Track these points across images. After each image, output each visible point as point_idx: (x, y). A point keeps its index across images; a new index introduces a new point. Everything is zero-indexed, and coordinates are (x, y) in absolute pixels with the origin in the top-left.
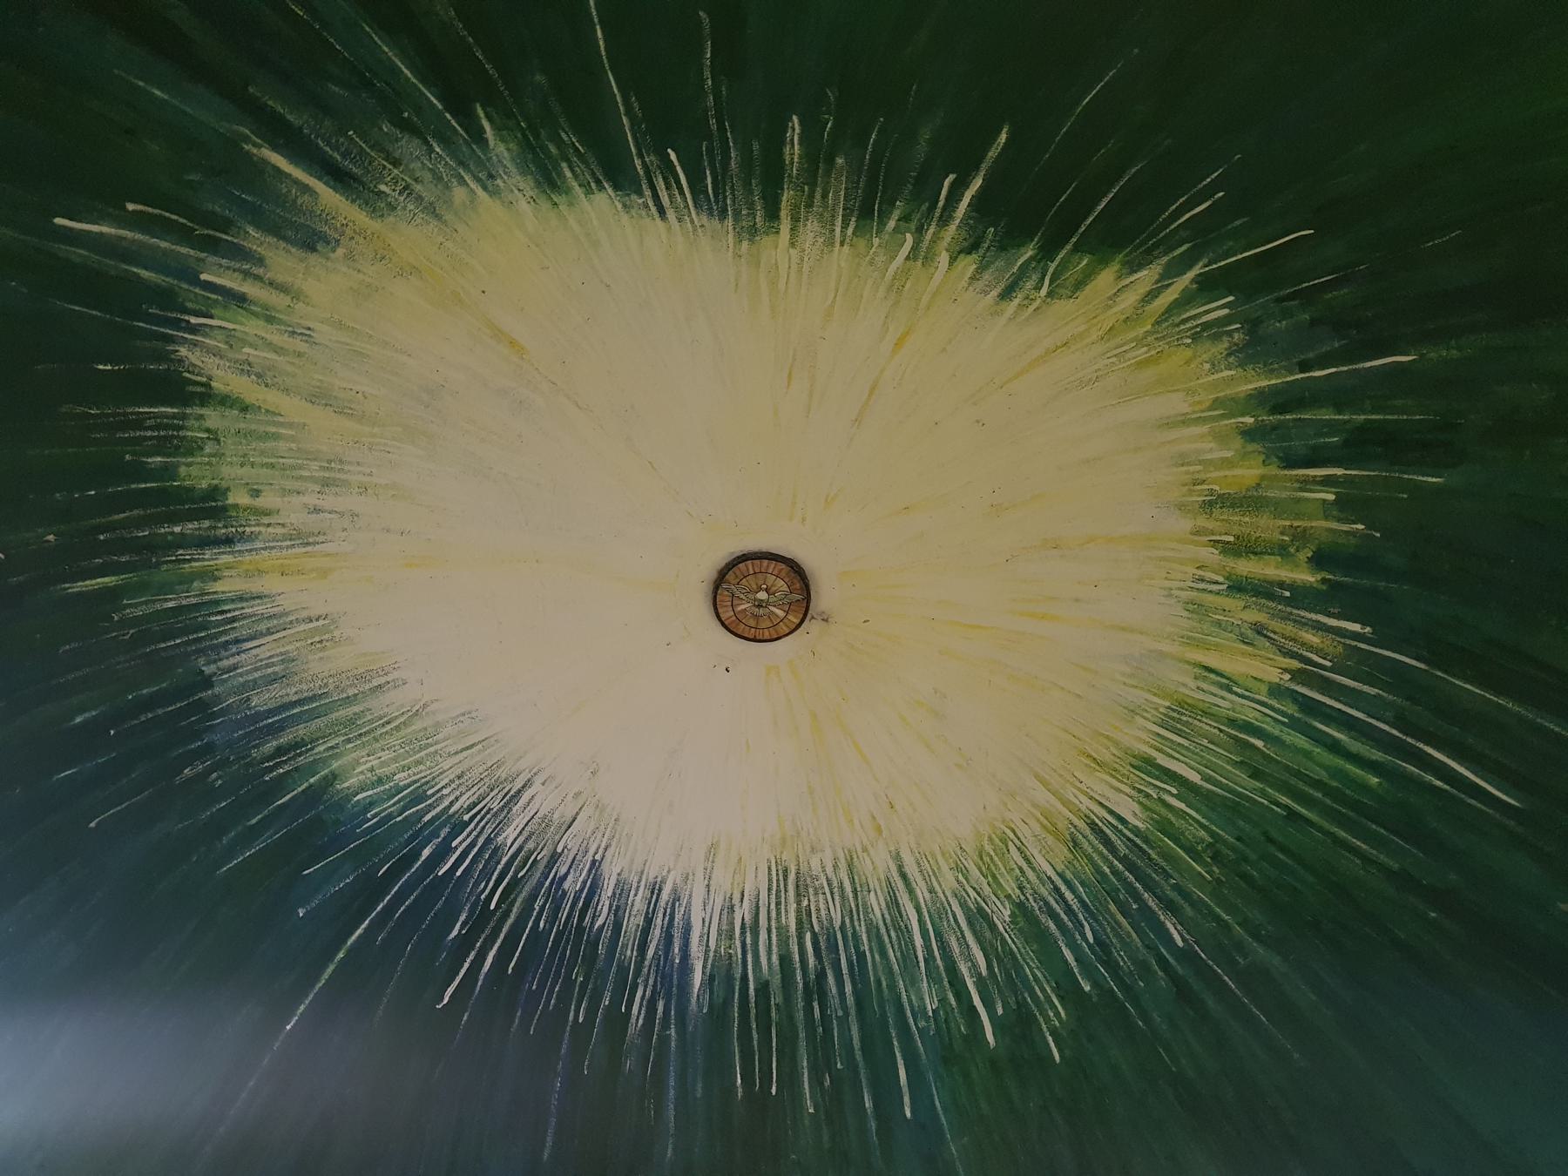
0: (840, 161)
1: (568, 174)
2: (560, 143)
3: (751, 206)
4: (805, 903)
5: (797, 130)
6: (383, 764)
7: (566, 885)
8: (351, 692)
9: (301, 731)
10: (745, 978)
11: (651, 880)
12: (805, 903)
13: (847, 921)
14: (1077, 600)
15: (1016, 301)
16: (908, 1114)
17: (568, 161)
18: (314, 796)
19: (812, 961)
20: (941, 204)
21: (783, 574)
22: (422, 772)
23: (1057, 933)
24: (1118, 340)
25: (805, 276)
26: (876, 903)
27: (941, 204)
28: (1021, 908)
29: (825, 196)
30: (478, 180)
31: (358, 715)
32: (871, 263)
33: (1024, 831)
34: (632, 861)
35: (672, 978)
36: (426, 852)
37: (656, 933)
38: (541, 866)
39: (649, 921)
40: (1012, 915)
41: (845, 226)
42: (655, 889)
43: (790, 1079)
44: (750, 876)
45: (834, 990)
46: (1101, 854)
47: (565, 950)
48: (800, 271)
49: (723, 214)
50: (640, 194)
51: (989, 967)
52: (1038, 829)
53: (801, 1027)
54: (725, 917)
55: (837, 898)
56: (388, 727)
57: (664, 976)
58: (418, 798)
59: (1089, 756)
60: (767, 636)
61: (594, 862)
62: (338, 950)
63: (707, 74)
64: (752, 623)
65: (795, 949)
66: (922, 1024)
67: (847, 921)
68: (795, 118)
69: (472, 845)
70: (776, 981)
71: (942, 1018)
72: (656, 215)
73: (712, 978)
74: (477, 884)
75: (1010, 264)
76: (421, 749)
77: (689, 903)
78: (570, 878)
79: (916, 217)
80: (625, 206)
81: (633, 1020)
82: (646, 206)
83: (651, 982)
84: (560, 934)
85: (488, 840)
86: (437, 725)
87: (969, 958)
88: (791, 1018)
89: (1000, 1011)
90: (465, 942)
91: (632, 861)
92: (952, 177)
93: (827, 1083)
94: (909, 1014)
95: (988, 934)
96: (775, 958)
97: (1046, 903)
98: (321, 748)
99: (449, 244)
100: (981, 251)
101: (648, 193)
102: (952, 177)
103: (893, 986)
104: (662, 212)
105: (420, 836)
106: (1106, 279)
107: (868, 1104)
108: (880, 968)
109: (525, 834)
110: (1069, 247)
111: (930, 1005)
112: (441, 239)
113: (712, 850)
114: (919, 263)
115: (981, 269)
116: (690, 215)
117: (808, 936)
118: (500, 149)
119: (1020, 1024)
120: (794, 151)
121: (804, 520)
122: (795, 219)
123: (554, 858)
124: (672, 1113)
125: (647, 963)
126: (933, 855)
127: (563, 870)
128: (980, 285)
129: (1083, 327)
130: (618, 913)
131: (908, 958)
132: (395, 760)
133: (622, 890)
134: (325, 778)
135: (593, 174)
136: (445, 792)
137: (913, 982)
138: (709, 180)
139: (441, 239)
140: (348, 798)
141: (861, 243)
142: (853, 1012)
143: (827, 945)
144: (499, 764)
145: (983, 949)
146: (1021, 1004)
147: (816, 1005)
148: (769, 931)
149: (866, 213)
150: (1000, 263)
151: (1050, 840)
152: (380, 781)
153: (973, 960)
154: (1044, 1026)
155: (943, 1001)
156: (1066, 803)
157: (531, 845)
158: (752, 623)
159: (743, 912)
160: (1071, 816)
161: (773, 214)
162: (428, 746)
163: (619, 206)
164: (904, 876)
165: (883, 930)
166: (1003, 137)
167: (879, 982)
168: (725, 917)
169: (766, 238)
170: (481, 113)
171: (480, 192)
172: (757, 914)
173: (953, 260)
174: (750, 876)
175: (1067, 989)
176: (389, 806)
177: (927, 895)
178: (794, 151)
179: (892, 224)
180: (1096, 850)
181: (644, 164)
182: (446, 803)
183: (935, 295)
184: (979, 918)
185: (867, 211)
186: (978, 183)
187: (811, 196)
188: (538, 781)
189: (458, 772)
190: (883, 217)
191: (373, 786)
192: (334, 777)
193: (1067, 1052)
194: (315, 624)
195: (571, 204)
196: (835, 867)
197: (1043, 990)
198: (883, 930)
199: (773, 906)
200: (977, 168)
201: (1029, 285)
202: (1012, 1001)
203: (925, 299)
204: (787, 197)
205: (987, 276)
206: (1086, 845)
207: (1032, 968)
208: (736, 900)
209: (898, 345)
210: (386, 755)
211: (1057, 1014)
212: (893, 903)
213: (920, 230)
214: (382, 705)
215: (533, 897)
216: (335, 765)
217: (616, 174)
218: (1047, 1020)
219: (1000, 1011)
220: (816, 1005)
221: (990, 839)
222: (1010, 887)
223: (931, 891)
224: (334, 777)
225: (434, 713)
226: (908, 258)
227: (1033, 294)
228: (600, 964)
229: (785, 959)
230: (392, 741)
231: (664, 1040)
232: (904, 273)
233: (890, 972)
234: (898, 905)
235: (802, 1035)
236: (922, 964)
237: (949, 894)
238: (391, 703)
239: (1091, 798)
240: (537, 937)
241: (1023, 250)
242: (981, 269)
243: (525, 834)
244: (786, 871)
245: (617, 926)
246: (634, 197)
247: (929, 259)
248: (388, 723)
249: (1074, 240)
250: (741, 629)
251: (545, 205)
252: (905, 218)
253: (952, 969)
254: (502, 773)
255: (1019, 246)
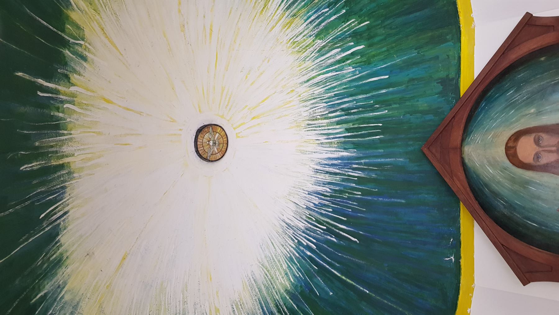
0: (37, 144)
1: (55, 256)
2: (43, 264)
3: (59, 177)
4: (319, 117)
5: (26, 166)
6: (281, 274)
7: (317, 203)
8: (257, 290)
9: (272, 305)
10: (344, 137)
11: (313, 173)
12: (319, 117)
13: (324, 101)
14: (204, 17)
15: (87, 54)
16: (387, 77)
17: (49, 258)
18: (293, 296)
19: (338, 113)
20: (50, 95)
21: (202, 136)
22: (282, 260)
23: (326, 22)
24: (99, 6)
25: (86, 147)
26: (318, 90)
27: (50, 95)
28: (317, 36)
29: (52, 146)
30: (61, 291)
31: (265, 286)
32: (77, 120)
33: (291, 35)
34: (307, 181)
35: (346, 163)
36: (309, 253)
37: (332, 170)
38: (311, 212)
39: (327, 172)
40: (320, 39)
41: (63, 135)
42: (317, 171)
43: (377, 119)
44: (310, 137)
45: (347, 105)
46: (298, 5)
47: (338, 201)
48: (83, 149)
49: (64, 188)
50: (59, 224)
51: (337, 48)
52: (290, 30)
53: (360, 116)
54: (325, 146)
55: (316, 105)
56: (268, 274)
57: (345, 166)
58: (291, 259)
59: (262, 10)
60: (225, 139)
61: (308, 194)
62: (347, 282)
63: (7, 213)
64: (221, 145)
65: (334, 120)
66: (357, 72)
67: (324, 101)
68: (21, 168)
69: (305, 238)
70: (345, 126)
71: (356, 65)
72: (67, 215)
73: (345, 149)
74: (318, 234)
75: (72, 60)
76: (275, 261)
77: (320, 159)
78: (314, 202)
79: (57, 105)
80: (65, 229)
81: (359, 175)
82: (64, 220)
83: (347, 170)
84: (333, 203)
85: (303, 232)
86: (266, 257)
87: (335, 55)
88: (357, 120)
89: (352, 43)
90: (337, 236)
91: (307, 181)
92: (39, 93)
93: (377, 106)
94: (354, 77)
95: (327, 48)
96: (338, 127)
97: (315, 26)
98: (277, 297)
99: (88, 295)
100: (68, 73)
101: (58, 221)
102: (39, 93)
103: (345, 84)
104: (66, 213)
105: (303, 256)
106: (74, 16)
107: (384, 91)
108: (339, 88)
109: (300, 219)
110: (63, 35)
111: (351, 69)
112: (87, 299)
113: (303, 152)
114: (75, 99)
115: (75, 71)
116: (66, 201)
117: (330, 115)
118: (48, 287)
119: (357, 36)
120: (35, 165)
121: (181, 130)
122: (63, 157)
123: (308, 208)
124: (389, 160)
125: (341, 172)
126: (300, 70)
127: (312, 205)
128: (82, 71)
129: (95, 22)
130: (324, 184)
131: (336, 78)
132: (279, 270)
133: (318, 183)
134: (287, 294)
135: (53, 246)
136: (288, 250)
137: (343, 76)
138: (51, 197)
139: (87, 299)
140: (293, 284)
141: (70, 126)
142: (354, 98)
143: (332, 108)
144: (278, 232)
145: (332, 50)
146: (350, 36)
147: (352, 111)
148: (329, 129)
149: (57, 127)
150: (72, 64)
151: (293, 25)
152: (286, 274)
153: (336, 54)
154: (357, 27)
155: (349, 65)
156: (280, 19)
157: (304, 217)
158: (221, 145)
159: (323, 139)
160: (285, 17)
161: (62, 167)
162: (273, 259)
163: (65, 231)
164: (308, 81)
165: (327, 88)
166: (20, 74)
167: (344, 89)
168: (325, 146)
169: (72, 167)
170: (34, 300)
171: (65, 289)
172: (323, 134)
173: (73, 85)
174: (310, 137)
175: (345, 18)
176: (294, 269)
177: (314, 71)
178: (35, 165)
179: (61, 115)
180: (296, 7)
181: (47, 226)
182: (292, 249)
183: (88, 90)
184: (321, 52)
185: (56, 127)
186: (40, 81)
187: (53, 152)
188: (282, 217)
189: (281, 246)
190: (59, 119)
191: (288, 276)
192: (287, 291)
193: (366, 19)
194: (235, 309)
195: (67, 251)
196: (306, 106)
197: (345, 27)
198: (327, 88)
199: (320, 128)
200: (34, 82)
201: (80, 49)
202: (349, 39)
203: (92, 94)
204: (54, 163)
205: (78, 68)
206: (295, 11)
207: (337, 32)
208: (319, 142)
209: (109, 101)
210: (278, 273)
211: (353, 22)
212: (317, 84)
213: (62, 102)
214: (261, 279)
215: (321, 214)
216: (282, 291)
217: (52, 237)
218: (355, 26)
219: (352, 43)
220: (352, 111)
221: (293, 48)
222: (310, 40)
223: (313, 70)
224: (287, 291)
225: (262, 259)
226: (74, 105)
227: (84, 47)
228: (342, 188)
229: (338, 123)
230: (272, 272)
231: (365, 164)
232: (80, 105)
233: (340, 84)
234: (318, 83)
235: (362, 116)
236: (338, 73)
237: (314, 63)
238: (259, 274)
239: (278, 9)
240: (334, 211)
241: (66, 55)
242: (75, 71)
243: (300, 219)
244: (308, 125)
245: (329, 183)
246: (61, 226)
247: (73, 95)
248: (266, 275)
249: (60, 33)
250: (224, 150)
251: (68, 261)
252: (58, 109)
253: (339, 62)
254: (280, 230)
255: (65, 57)
